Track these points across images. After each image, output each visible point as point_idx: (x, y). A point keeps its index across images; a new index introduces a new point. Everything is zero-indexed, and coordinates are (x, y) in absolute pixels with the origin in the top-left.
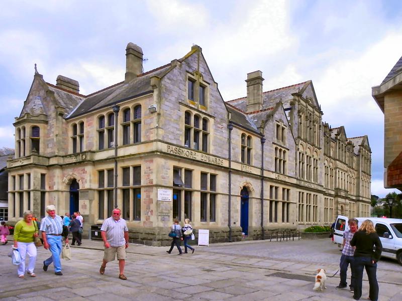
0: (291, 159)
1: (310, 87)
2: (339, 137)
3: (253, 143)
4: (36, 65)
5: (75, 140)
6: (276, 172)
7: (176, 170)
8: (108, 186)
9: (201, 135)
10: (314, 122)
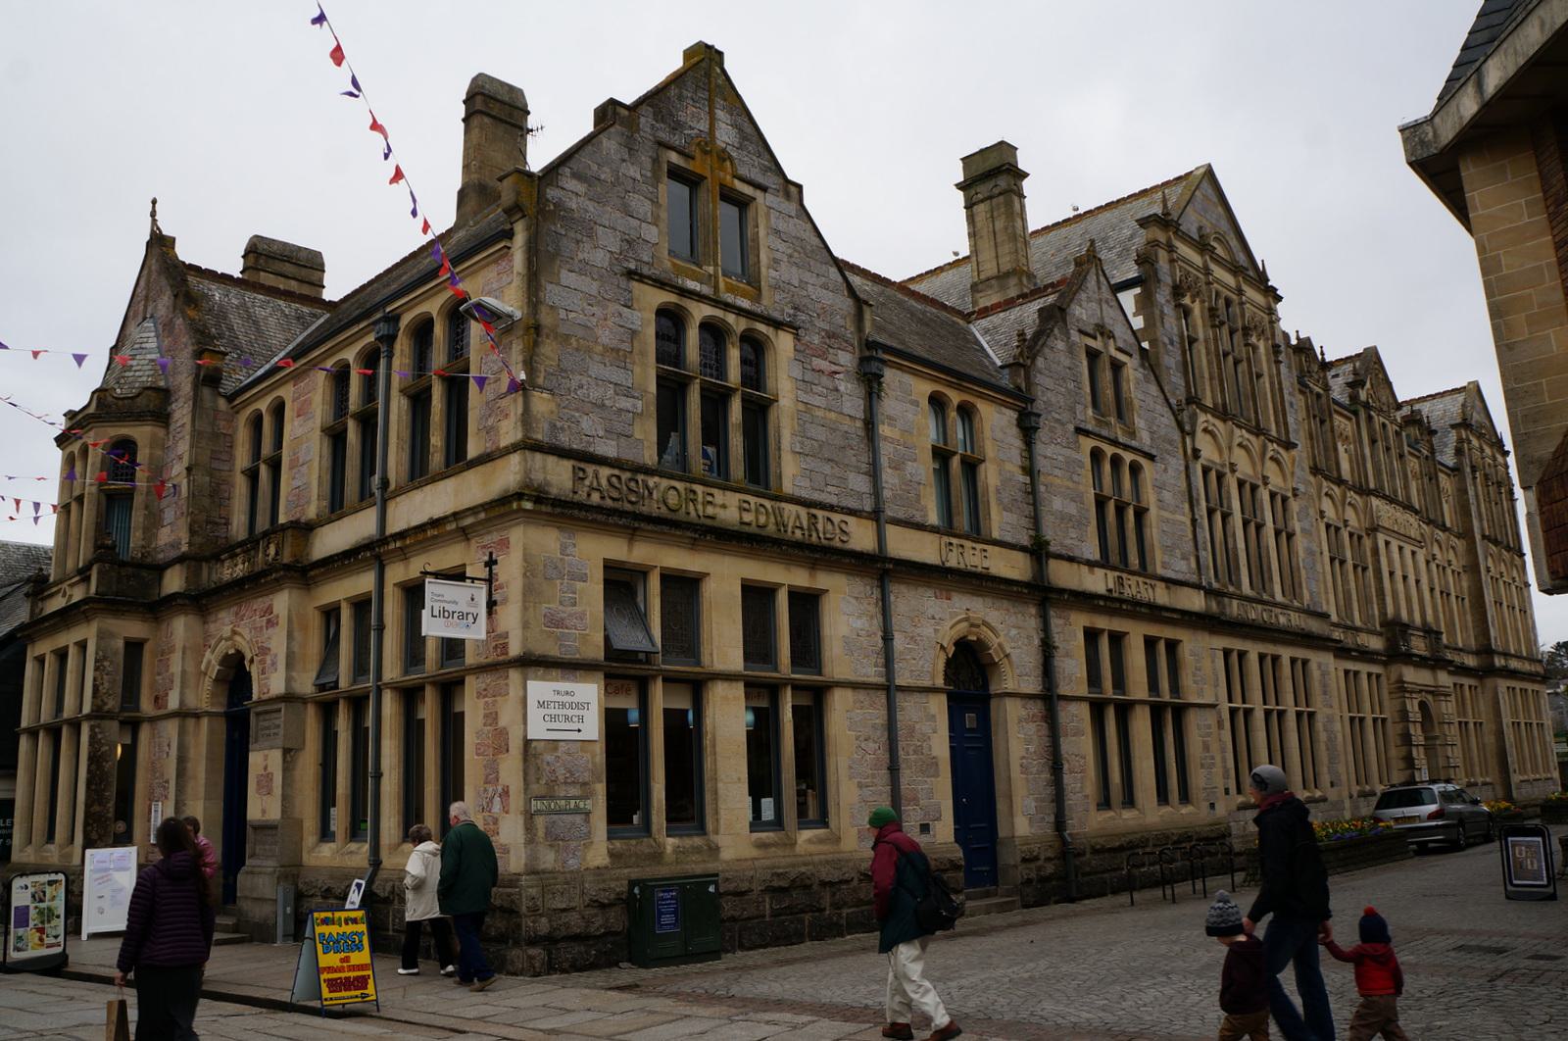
0: (1167, 496)
1: (1210, 191)
2: (1363, 395)
3: (987, 433)
4: (154, 202)
6: (1104, 563)
7: (621, 584)
9: (1130, 513)
10: (1246, 331)
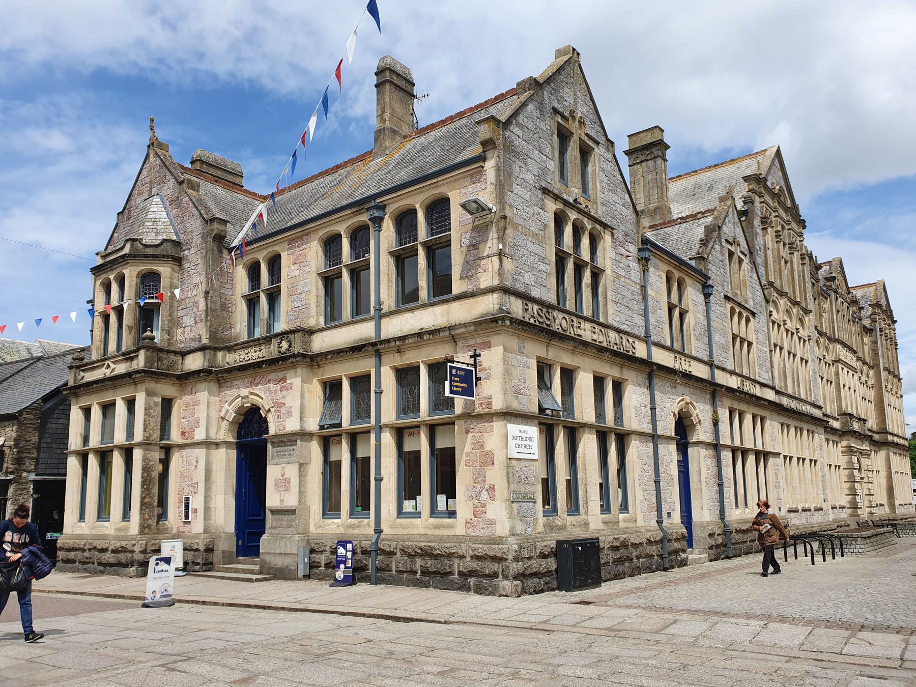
0: (760, 336)
5: (252, 303)
8: (351, 424)
